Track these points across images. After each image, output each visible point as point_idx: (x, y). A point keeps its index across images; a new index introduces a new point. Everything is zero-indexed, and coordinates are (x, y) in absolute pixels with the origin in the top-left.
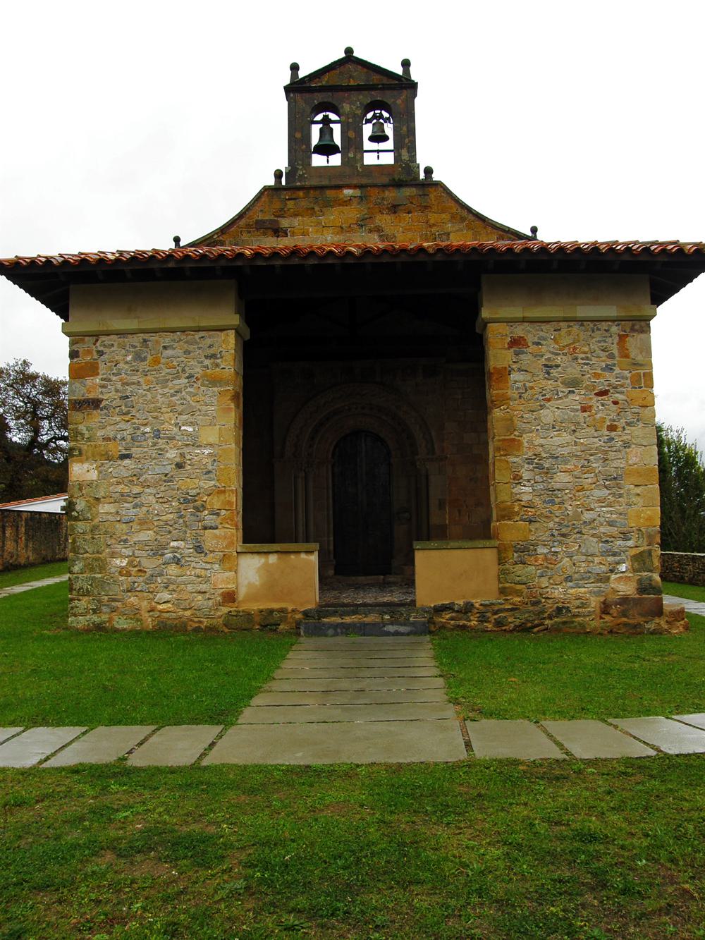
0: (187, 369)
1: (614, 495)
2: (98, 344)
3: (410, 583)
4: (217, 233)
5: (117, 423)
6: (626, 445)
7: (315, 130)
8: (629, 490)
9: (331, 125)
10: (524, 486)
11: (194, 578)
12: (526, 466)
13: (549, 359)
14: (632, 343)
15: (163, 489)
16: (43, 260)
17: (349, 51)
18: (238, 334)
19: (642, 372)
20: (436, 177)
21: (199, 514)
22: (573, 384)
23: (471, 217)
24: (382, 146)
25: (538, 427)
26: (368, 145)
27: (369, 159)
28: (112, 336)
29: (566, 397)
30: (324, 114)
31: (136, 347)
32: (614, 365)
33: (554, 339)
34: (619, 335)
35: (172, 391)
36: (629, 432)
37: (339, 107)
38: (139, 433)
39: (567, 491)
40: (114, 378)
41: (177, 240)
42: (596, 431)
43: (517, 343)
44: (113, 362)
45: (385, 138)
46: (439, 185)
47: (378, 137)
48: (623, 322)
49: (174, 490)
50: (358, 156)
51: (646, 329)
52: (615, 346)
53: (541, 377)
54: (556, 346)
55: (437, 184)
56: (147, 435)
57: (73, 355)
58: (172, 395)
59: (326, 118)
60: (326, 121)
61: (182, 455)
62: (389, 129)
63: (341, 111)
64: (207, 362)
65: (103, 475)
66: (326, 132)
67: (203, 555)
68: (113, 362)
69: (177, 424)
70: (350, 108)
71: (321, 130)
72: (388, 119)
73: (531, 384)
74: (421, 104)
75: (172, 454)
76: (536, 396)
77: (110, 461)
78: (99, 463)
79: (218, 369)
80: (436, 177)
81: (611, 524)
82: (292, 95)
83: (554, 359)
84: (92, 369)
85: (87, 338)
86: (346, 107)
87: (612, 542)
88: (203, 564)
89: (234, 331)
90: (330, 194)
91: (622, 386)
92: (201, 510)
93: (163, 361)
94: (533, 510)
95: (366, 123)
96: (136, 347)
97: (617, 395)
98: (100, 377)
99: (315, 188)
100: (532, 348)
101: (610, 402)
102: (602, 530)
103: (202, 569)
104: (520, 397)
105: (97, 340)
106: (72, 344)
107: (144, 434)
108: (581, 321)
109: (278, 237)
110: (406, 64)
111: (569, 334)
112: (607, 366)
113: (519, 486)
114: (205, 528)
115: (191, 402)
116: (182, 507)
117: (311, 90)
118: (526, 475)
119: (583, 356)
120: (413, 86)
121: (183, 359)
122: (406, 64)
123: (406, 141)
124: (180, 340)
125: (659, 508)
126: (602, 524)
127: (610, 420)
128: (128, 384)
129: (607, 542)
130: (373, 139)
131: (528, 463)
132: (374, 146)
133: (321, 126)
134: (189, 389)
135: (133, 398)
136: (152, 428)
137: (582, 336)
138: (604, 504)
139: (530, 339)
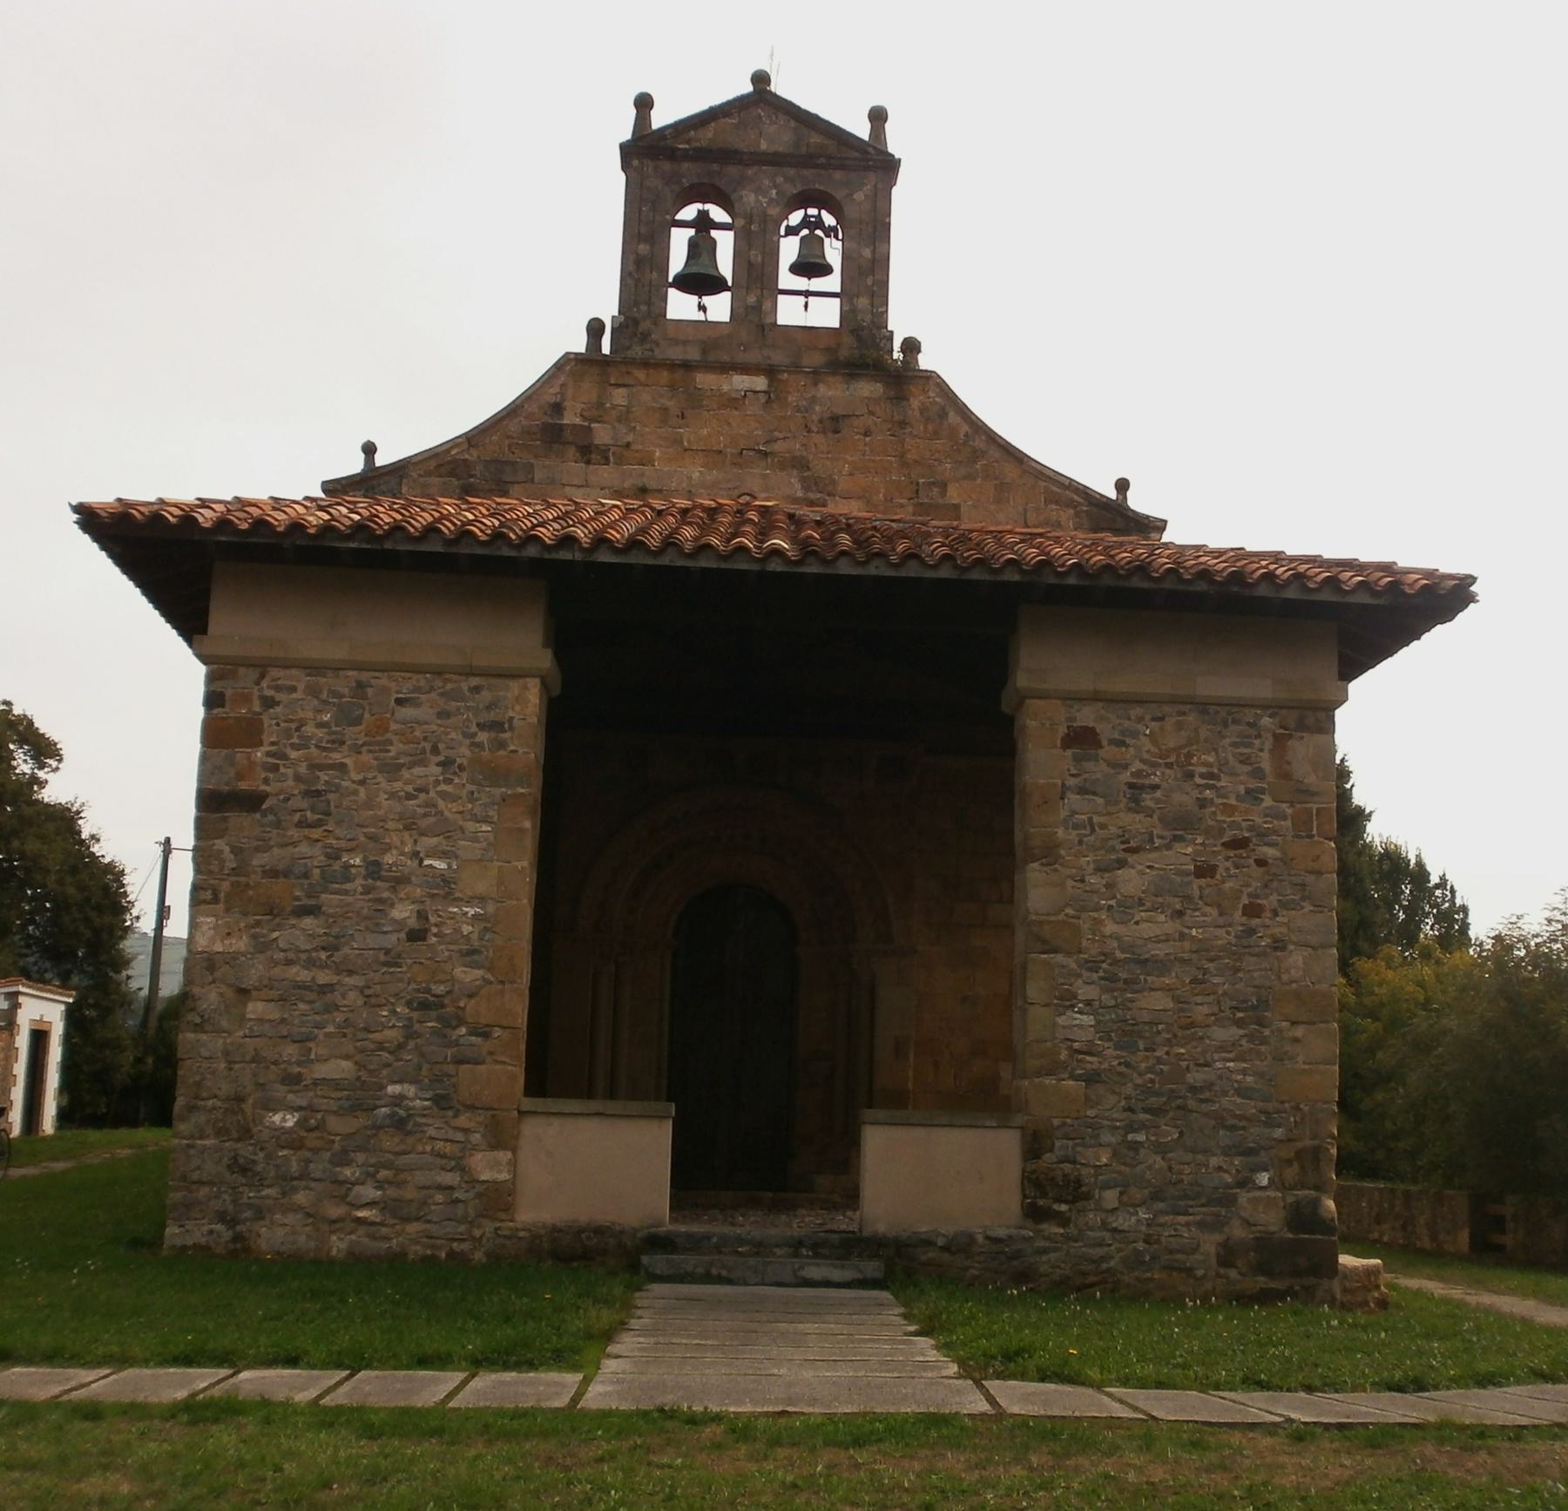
0: (441, 746)
1: (1251, 1037)
2: (264, 684)
3: (852, 1198)
4: (457, 445)
5: (294, 844)
6: (1279, 945)
7: (680, 239)
8: (1280, 1030)
9: (714, 233)
10: (1080, 1012)
11: (430, 1159)
12: (1086, 974)
13: (1138, 774)
14: (1301, 749)
15: (377, 977)
16: (177, 512)
17: (761, 79)
18: (544, 684)
19: (1315, 806)
20: (925, 362)
21: (448, 1031)
22: (1181, 825)
23: (995, 453)
24: (817, 284)
25: (1113, 902)
26: (787, 280)
27: (789, 312)
28: (294, 672)
29: (1168, 847)
30: (699, 206)
31: (343, 696)
32: (1262, 791)
33: (1152, 737)
34: (1275, 736)
35: (409, 789)
36: (1285, 920)
37: (733, 197)
38: (337, 866)
39: (1160, 1027)
40: (294, 755)
41: (369, 450)
42: (1221, 914)
43: (1081, 740)
44: (292, 721)
45: (825, 270)
46: (931, 378)
47: (810, 266)
48: (1284, 712)
49: (401, 980)
50: (767, 305)
51: (1328, 727)
52: (1265, 755)
53: (1122, 805)
54: (1153, 749)
55: (929, 378)
56: (353, 871)
57: (213, 700)
58: (409, 797)
59: (703, 215)
60: (703, 224)
61: (422, 916)
62: (833, 252)
63: (737, 205)
64: (483, 737)
65: (262, 946)
66: (701, 248)
67: (450, 1113)
68: (292, 721)
69: (415, 854)
70: (758, 201)
71: (693, 244)
72: (834, 229)
73: (1102, 819)
74: (907, 203)
75: (402, 912)
76: (1110, 843)
77: (275, 916)
78: (252, 919)
79: (502, 752)
80: (925, 362)
81: (1242, 1092)
82: (636, 163)
83: (1149, 775)
84: (250, 733)
85: (242, 670)
86: (749, 198)
87: (1244, 1128)
88: (451, 1132)
89: (537, 681)
90: (704, 380)
91: (1275, 832)
92: (454, 1023)
93: (394, 727)
94: (1094, 1059)
95: (787, 235)
96: (343, 696)
97: (1265, 849)
98: (266, 748)
99: (672, 366)
100: (1108, 751)
101: (1251, 861)
102: (1225, 1102)
103: (447, 1140)
104: (1080, 842)
105: (262, 676)
106: (211, 679)
107: (347, 867)
108: (1203, 706)
109: (588, 462)
110: (878, 117)
111: (1179, 726)
112: (1248, 791)
113: (1069, 1013)
114: (460, 1062)
115: (447, 813)
116: (415, 1015)
117: (672, 155)
118: (1084, 992)
119: (1204, 770)
120: (888, 167)
121: (435, 727)
122: (878, 117)
123: (867, 282)
124: (432, 689)
125: (1337, 1068)
126: (1225, 1093)
127: (1249, 895)
128: (322, 767)
129: (1233, 1128)
130: (798, 269)
131: (1090, 970)
132: (801, 283)
133: (692, 232)
134: (443, 787)
135: (331, 796)
136: (364, 859)
137: (1204, 732)
138: (1231, 1056)
139: (1105, 731)
